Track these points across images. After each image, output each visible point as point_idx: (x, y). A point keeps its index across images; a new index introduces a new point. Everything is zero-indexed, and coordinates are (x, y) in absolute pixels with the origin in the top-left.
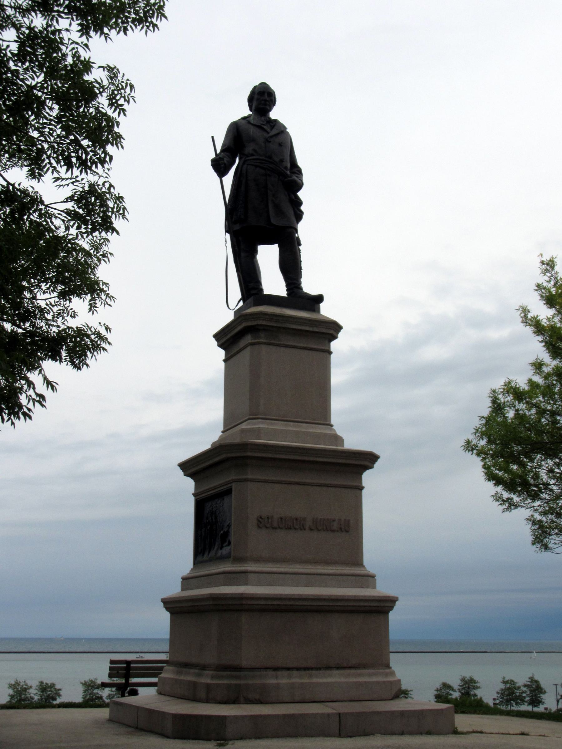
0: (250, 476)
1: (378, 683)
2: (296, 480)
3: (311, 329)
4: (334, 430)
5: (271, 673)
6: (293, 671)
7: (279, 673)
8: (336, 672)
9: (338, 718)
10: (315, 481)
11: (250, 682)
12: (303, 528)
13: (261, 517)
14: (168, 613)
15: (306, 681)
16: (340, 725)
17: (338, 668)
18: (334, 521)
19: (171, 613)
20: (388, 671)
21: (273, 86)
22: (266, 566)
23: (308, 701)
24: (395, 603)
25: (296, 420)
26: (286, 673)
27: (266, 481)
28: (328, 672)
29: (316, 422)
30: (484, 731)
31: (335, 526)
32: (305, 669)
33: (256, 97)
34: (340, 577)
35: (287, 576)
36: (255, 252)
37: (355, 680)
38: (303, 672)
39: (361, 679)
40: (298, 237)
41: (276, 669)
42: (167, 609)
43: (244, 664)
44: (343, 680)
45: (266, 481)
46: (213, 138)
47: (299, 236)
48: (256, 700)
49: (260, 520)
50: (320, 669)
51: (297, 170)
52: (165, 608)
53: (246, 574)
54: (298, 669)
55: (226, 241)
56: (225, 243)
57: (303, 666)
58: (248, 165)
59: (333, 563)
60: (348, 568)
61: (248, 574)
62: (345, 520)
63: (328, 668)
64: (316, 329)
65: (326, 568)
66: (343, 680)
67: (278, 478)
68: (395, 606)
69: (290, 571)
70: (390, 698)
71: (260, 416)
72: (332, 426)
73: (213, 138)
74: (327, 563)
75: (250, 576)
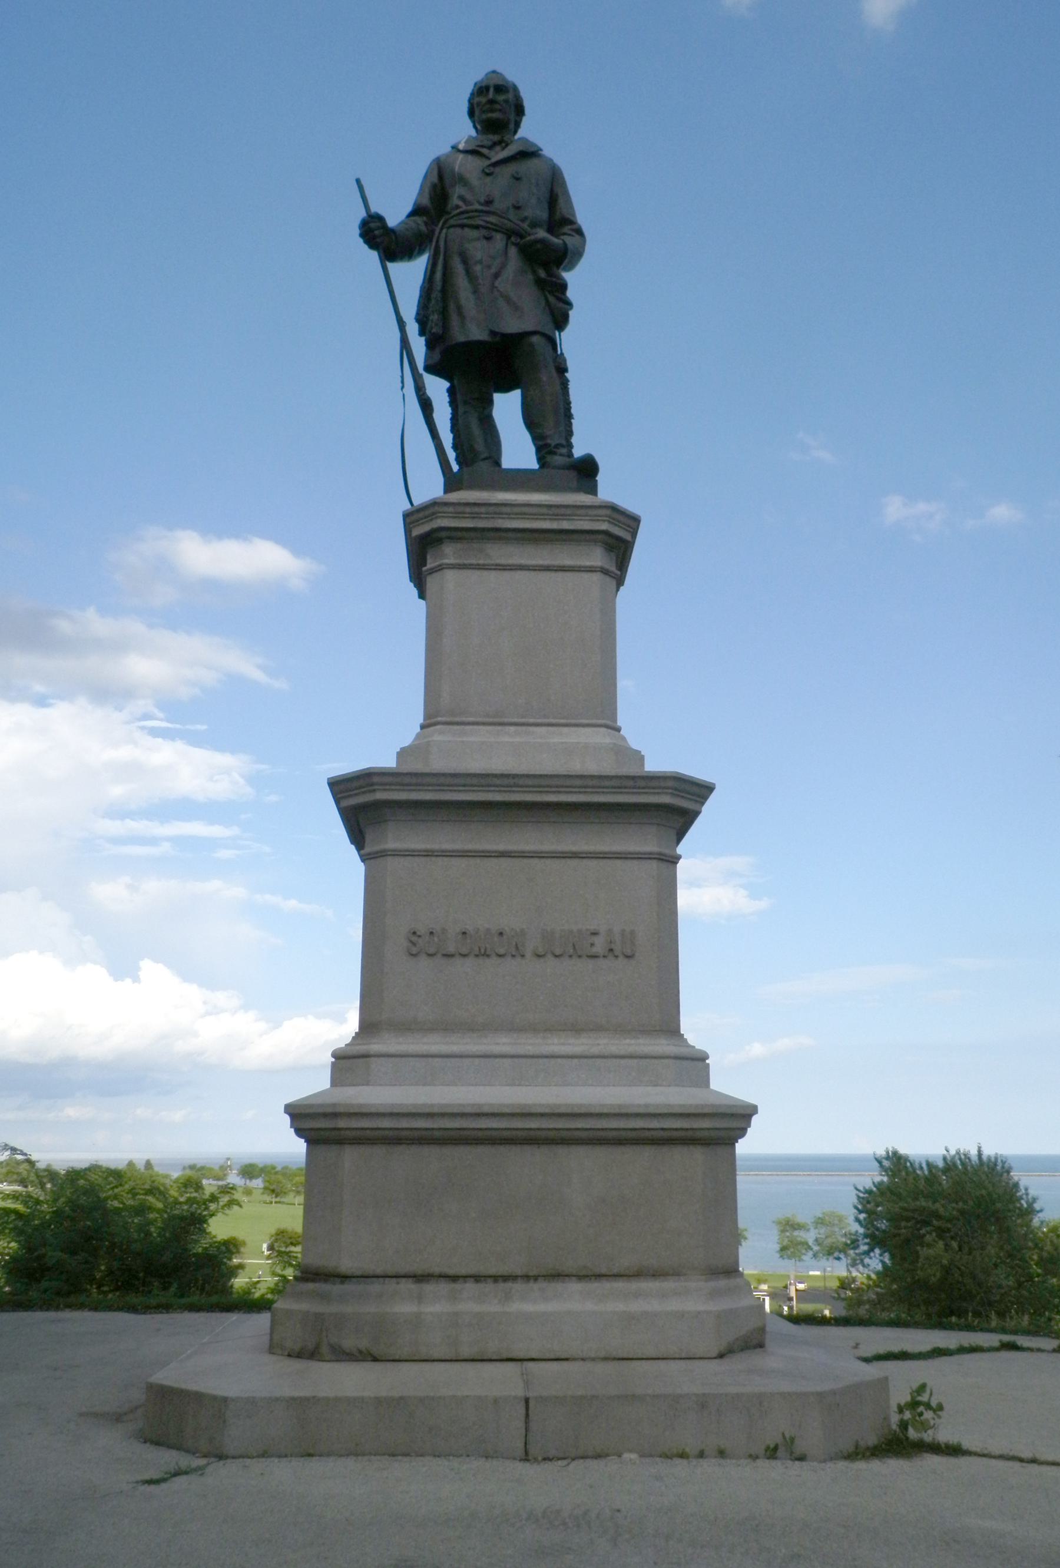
0: (391, 845)
1: (681, 1315)
2: (501, 847)
3: (555, 525)
4: (624, 739)
5: (407, 1286)
6: (465, 1282)
7: (429, 1288)
8: (574, 1287)
9: (522, 1411)
10: (547, 847)
11: (349, 1309)
12: (518, 953)
13: (414, 933)
14: (303, 1140)
15: (493, 1307)
16: (527, 1430)
17: (581, 1277)
18: (595, 934)
19: (307, 1141)
20: (733, 1282)
21: (512, 75)
22: (425, 1040)
23: (495, 1357)
24: (751, 1119)
25: (523, 720)
26: (444, 1287)
27: (428, 854)
28: (558, 1286)
29: (573, 721)
30: (966, 1445)
31: (599, 947)
32: (496, 1278)
33: (512, 117)
34: (599, 1061)
35: (467, 1062)
36: (490, 402)
37: (620, 1307)
38: (489, 1287)
39: (636, 1306)
40: (562, 354)
41: (421, 1278)
42: (299, 1132)
43: (346, 1265)
44: (590, 1306)
45: (428, 854)
46: (358, 181)
47: (564, 351)
48: (360, 1352)
49: (414, 939)
50: (536, 1278)
51: (573, 230)
52: (292, 1130)
53: (368, 1059)
54: (477, 1278)
55: (402, 382)
56: (401, 385)
57: (493, 1271)
58: (448, 228)
59: (592, 1030)
60: (628, 1041)
61: (372, 1059)
62: (623, 931)
63: (557, 1276)
64: (565, 525)
65: (572, 1041)
66: (590, 1306)
67: (458, 846)
68: (750, 1127)
69: (474, 1050)
70: (714, 1355)
71: (439, 719)
72: (618, 730)
73: (358, 181)
74: (576, 1029)
75: (374, 1063)
